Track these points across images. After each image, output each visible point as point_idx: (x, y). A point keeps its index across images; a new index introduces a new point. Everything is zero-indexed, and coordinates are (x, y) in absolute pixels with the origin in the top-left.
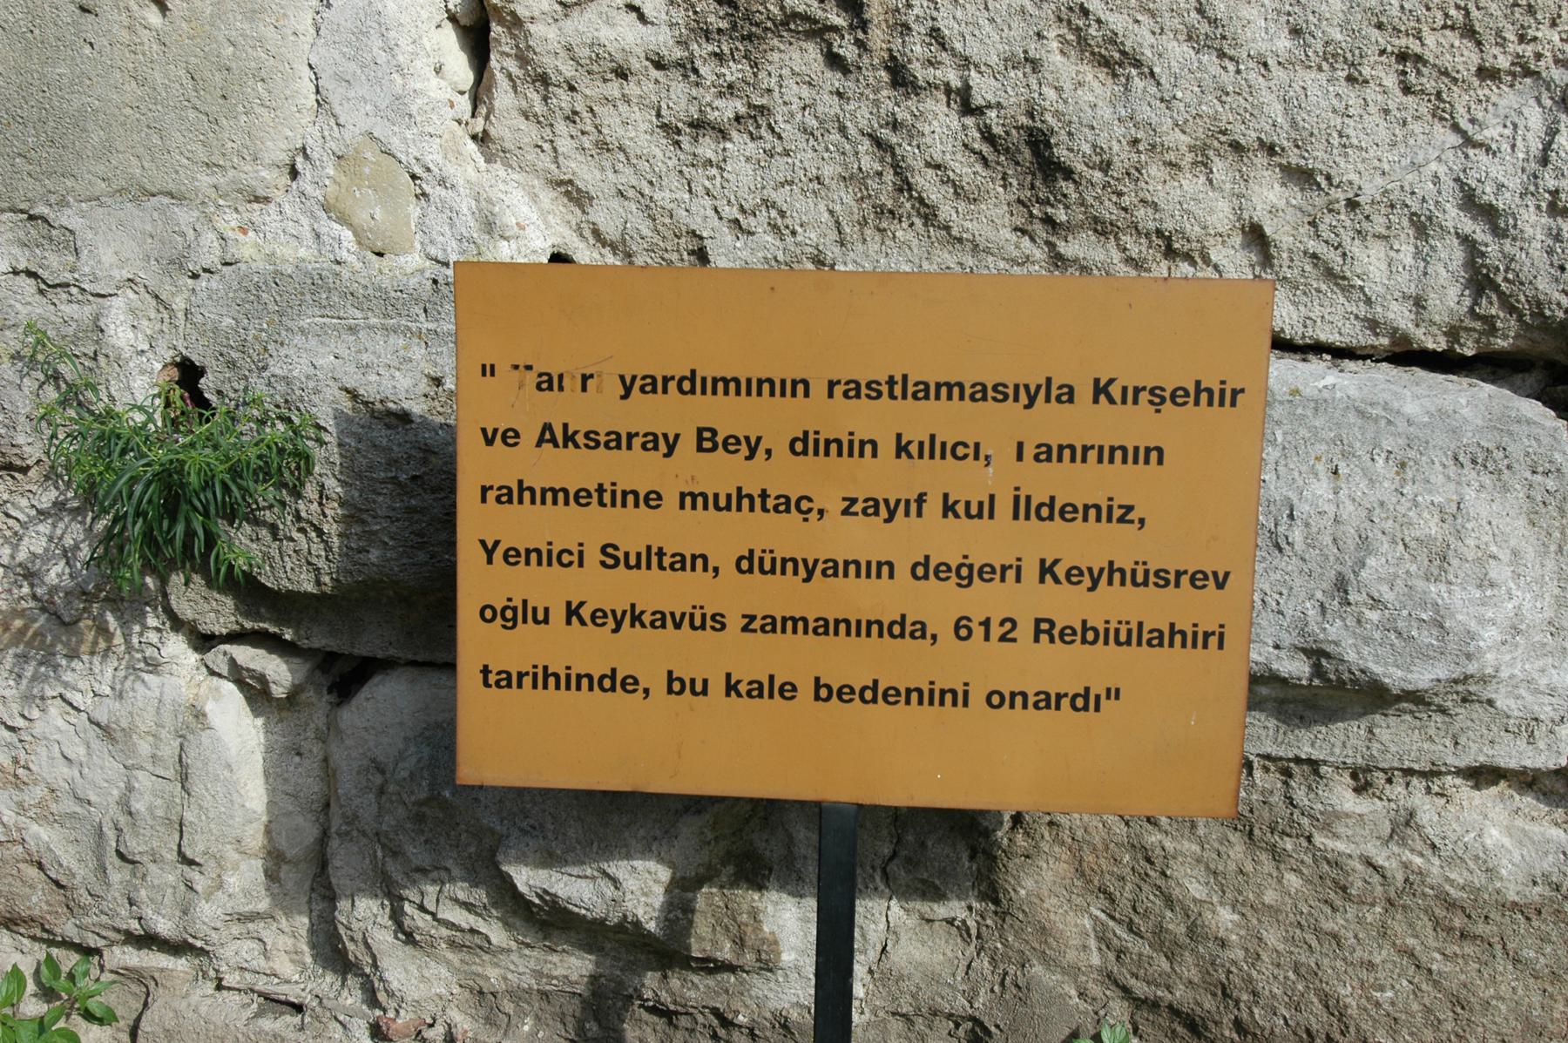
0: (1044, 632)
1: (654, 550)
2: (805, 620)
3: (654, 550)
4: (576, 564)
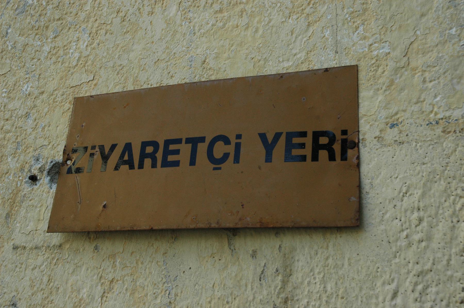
4: (231, 157)
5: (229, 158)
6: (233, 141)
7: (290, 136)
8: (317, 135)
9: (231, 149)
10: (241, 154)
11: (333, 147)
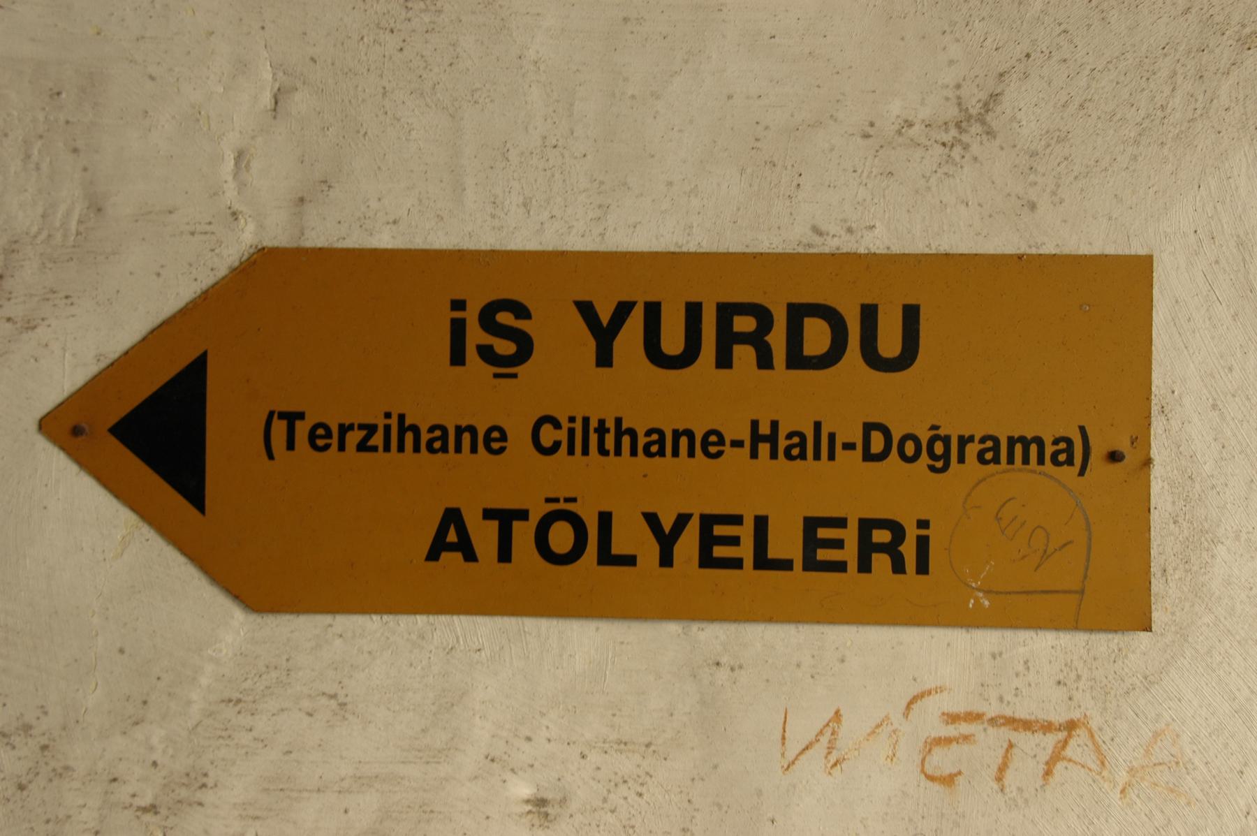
0: (881, 548)
1: (594, 424)
2: (1039, 442)
3: (594, 424)
4: (564, 447)
5: (562, 446)
6: (566, 425)
7: (708, 521)
8: (867, 526)
9: (562, 435)
10: (595, 249)
11: (767, 338)
